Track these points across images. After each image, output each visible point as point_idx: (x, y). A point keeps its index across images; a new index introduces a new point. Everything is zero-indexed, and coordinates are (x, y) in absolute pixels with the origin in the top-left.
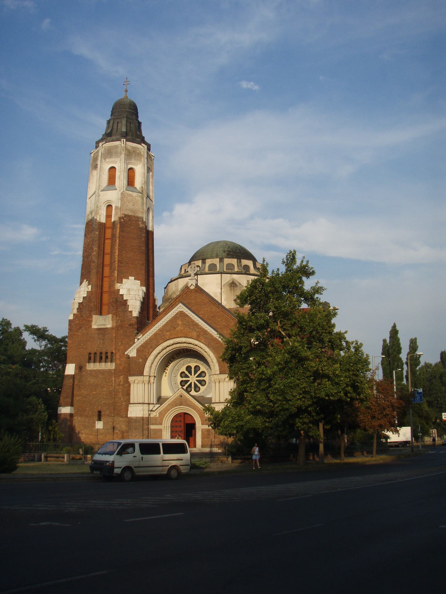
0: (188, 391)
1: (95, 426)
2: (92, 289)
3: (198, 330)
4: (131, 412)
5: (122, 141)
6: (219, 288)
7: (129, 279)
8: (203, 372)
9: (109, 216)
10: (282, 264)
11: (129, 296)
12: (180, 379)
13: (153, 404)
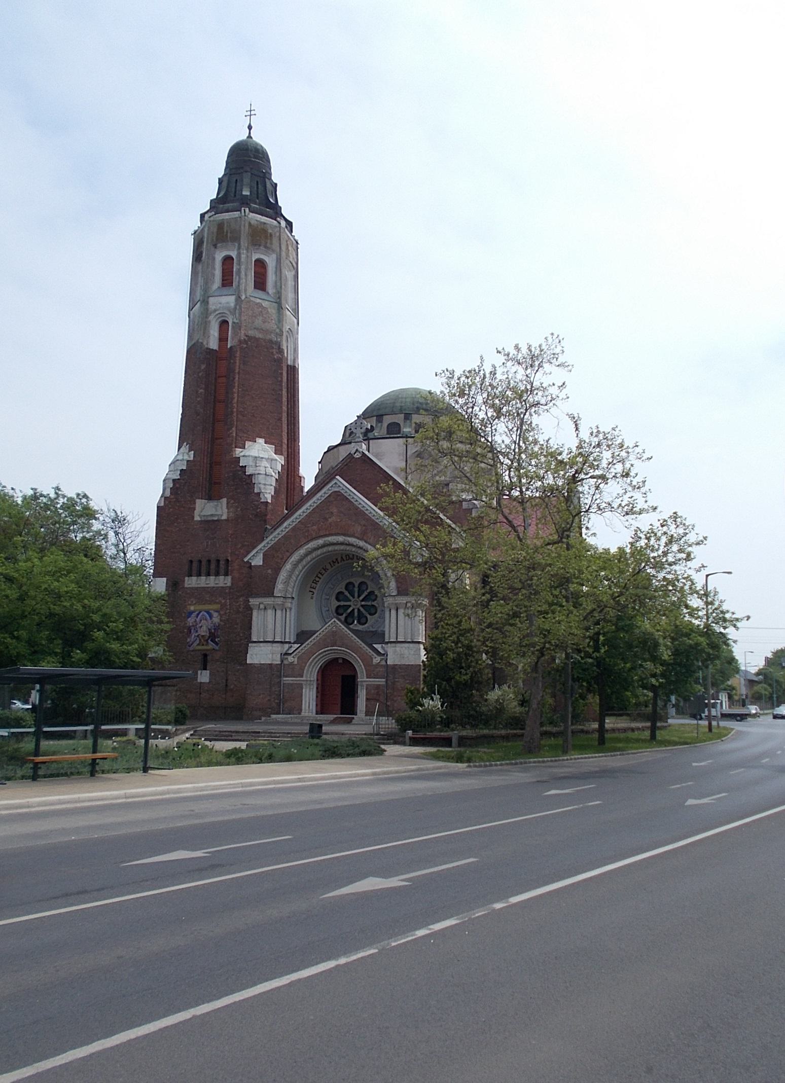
0: (347, 623)
2: (194, 457)
3: (363, 522)
4: (252, 655)
5: (243, 211)
6: (403, 460)
7: (255, 442)
8: (361, 584)
9: (223, 339)
11: (255, 469)
13: (289, 643)
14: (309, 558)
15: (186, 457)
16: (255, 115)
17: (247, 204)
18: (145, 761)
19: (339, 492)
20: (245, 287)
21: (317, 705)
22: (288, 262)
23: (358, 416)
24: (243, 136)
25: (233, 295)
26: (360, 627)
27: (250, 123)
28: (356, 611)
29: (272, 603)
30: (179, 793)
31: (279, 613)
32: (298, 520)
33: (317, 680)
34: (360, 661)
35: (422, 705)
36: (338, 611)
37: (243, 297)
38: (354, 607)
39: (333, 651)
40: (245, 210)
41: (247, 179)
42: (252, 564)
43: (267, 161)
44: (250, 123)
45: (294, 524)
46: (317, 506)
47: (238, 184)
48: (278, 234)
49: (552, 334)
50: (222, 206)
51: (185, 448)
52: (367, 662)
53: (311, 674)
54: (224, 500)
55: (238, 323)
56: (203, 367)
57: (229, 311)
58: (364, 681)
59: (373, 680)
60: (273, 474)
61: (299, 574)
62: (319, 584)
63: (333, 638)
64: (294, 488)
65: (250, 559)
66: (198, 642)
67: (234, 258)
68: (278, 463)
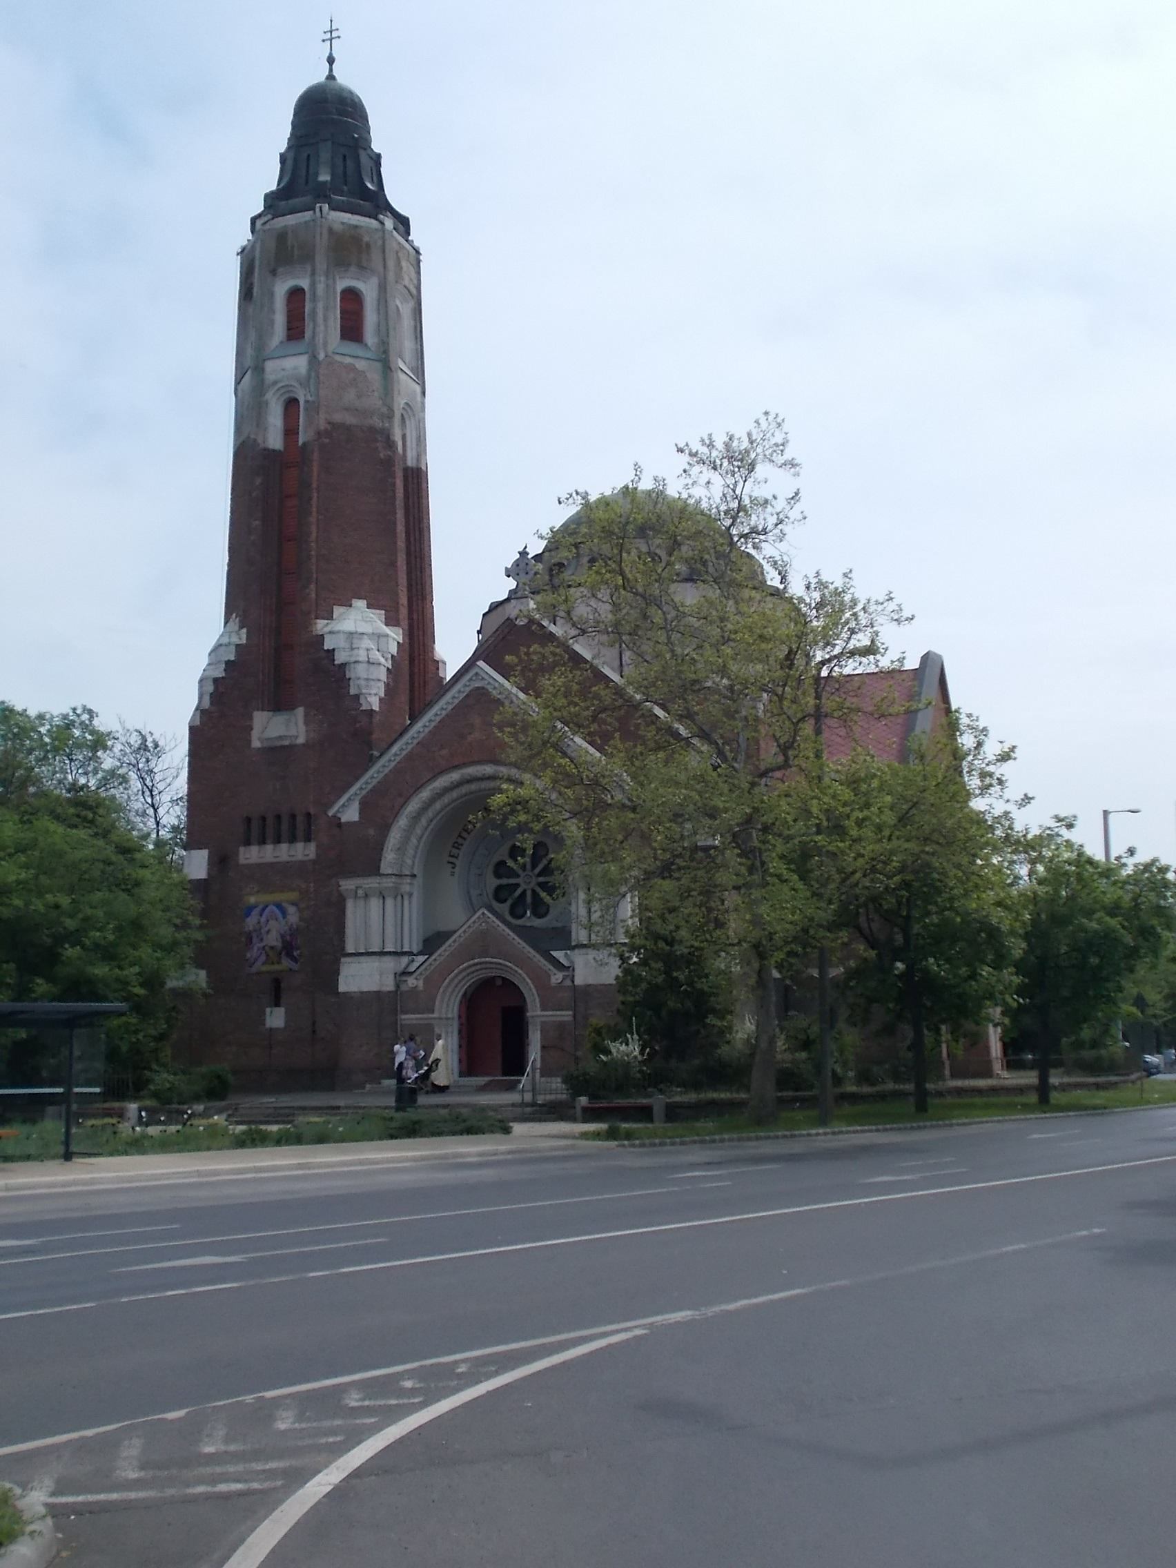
1: (263, 1022)
7: (351, 606)
9: (290, 431)
10: (1030, 796)
12: (493, 882)
13: (410, 953)
14: (438, 805)
15: (235, 640)
16: (339, 37)
17: (325, 196)
18: (67, 1143)
19: (483, 688)
20: (325, 337)
21: (460, 1061)
22: (400, 287)
23: (520, 553)
24: (320, 77)
25: (306, 353)
26: (537, 922)
27: (331, 54)
28: (529, 893)
29: (377, 885)
30: (92, 1184)
31: (390, 902)
32: (415, 742)
33: (460, 1017)
34: (529, 981)
35: (607, 1052)
36: (500, 894)
37: (321, 356)
38: (525, 887)
39: (484, 966)
40: (321, 207)
41: (325, 153)
42: (343, 820)
43: (361, 117)
44: (331, 54)
45: (410, 747)
46: (447, 715)
47: (312, 163)
48: (380, 243)
49: (766, 413)
50: (283, 203)
51: (235, 623)
52: (541, 982)
53: (448, 1007)
54: (300, 711)
55: (314, 402)
56: (258, 481)
57: (298, 381)
58: (538, 1016)
59: (551, 1013)
60: (382, 660)
61: (423, 834)
62: (463, 848)
63: (483, 943)
64: (425, 682)
65: (338, 811)
66: (263, 958)
67: (306, 290)
68: (391, 641)
